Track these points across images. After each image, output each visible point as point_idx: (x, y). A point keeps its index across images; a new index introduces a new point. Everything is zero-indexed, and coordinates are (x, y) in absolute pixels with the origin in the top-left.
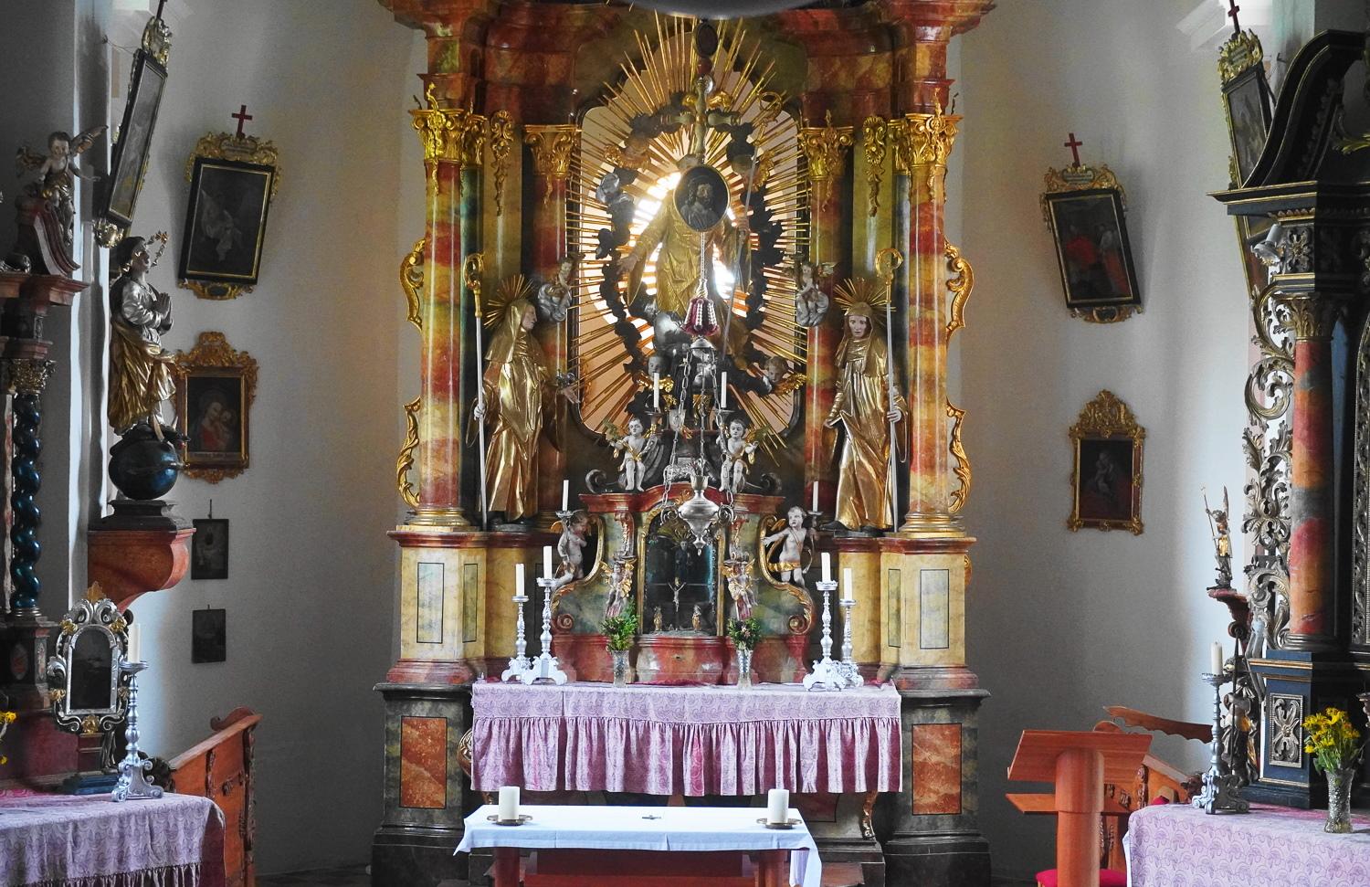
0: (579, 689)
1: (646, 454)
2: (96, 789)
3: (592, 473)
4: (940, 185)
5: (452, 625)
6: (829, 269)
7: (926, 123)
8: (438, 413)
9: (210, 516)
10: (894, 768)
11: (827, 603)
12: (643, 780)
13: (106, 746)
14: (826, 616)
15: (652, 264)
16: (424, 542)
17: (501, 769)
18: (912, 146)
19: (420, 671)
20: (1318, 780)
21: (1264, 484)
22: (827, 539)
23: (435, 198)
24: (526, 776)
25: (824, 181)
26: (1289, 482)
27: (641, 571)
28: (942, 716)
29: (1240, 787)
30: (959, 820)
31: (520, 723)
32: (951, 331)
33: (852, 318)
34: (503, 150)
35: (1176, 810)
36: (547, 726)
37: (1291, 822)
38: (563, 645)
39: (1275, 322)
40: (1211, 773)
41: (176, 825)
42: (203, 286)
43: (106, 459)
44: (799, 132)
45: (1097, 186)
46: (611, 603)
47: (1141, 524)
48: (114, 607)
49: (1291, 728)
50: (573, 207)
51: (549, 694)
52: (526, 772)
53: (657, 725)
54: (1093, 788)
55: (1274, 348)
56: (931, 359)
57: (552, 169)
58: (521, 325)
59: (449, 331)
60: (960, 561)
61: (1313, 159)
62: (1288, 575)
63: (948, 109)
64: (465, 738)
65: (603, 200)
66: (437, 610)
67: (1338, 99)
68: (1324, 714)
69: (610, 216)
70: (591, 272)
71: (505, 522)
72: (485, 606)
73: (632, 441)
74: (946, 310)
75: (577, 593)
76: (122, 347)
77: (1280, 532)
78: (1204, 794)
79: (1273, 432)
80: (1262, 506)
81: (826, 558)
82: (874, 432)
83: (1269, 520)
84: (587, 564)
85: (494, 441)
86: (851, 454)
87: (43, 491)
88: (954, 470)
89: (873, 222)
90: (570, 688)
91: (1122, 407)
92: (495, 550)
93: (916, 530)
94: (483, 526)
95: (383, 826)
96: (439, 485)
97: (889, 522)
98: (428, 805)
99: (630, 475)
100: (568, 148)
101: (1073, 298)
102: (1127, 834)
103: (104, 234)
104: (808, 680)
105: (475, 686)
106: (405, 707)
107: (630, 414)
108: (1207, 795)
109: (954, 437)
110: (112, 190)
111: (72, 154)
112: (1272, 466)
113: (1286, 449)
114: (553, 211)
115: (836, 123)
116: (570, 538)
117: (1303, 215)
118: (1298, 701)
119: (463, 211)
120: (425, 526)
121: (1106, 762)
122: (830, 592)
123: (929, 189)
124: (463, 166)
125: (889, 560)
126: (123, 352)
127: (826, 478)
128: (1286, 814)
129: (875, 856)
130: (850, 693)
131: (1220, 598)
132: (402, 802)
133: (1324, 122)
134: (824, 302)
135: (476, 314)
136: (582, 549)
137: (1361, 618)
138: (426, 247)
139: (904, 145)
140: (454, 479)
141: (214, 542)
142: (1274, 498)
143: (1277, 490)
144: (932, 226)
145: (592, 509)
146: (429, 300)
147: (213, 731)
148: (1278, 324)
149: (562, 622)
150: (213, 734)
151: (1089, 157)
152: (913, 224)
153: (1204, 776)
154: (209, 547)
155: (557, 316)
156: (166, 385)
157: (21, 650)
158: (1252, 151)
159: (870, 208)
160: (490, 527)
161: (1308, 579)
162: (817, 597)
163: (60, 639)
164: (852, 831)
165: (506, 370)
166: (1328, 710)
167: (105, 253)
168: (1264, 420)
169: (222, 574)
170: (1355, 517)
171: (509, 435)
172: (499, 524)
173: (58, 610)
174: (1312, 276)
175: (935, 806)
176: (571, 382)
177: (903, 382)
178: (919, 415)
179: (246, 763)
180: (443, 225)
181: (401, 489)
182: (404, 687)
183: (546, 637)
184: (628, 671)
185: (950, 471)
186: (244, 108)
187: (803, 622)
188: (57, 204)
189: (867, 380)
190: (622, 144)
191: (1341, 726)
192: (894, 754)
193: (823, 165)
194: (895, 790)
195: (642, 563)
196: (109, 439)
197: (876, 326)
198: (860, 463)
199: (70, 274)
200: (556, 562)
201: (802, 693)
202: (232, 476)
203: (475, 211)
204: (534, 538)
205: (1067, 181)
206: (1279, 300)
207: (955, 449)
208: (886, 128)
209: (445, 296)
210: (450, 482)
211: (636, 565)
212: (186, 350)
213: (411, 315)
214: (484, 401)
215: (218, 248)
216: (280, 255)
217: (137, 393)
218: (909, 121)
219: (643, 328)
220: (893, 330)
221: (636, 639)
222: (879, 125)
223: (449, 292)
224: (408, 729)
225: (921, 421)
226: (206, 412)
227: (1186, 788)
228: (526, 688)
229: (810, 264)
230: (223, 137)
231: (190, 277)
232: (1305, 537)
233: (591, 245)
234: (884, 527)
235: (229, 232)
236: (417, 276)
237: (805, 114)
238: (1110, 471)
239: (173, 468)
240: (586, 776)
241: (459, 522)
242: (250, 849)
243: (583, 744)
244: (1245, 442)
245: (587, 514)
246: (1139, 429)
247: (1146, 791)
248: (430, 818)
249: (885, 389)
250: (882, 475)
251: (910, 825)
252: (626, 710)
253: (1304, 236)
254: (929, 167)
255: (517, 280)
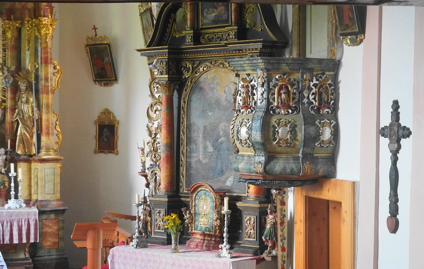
4: (51, 41)
6: (13, 68)
7: (46, 21)
10: (35, 234)
11: (13, 180)
14: (12, 184)
18: (41, 28)
20: (169, 236)
21: (153, 142)
22: (12, 158)
25: (11, 39)
26: (160, 141)
28: (52, 216)
29: (145, 239)
30: (58, 250)
32: (55, 89)
33: (21, 85)
35: (125, 247)
37: (161, 250)
39: (156, 90)
40: (136, 235)
44: (2, 22)
45: (103, 42)
47: (118, 152)
49: (161, 219)
54: (99, 240)
55: (156, 98)
56: (48, 99)
60: (58, 165)
61: (167, 39)
62: (160, 171)
63: (53, 16)
67: (175, 20)
68: (171, 215)
74: (54, 81)
77: (158, 157)
78: (134, 242)
79: (156, 125)
80: (152, 149)
81: (12, 165)
82: (29, 123)
83: (155, 153)
86: (21, 130)
88: (56, 135)
89: (28, 53)
91: (112, 114)
93: (43, 155)
97: (34, 153)
101: (95, 78)
102: (109, 256)
104: (6, 206)
108: (135, 242)
109: (56, 124)
112: (155, 136)
113: (159, 130)
115: (15, 20)
117: (164, 57)
118: (163, 211)
121: (103, 232)
122: (14, 176)
123: (47, 43)
125: (34, 165)
127: (13, 138)
128: (159, 247)
129: (30, 264)
130: (21, 210)
131: (142, 176)
133: (171, 27)
134: (11, 80)
137: (183, 184)
139: (38, 27)
142: (156, 146)
143: (157, 143)
144: (48, 55)
148: (157, 91)
151: (100, 33)
152: (41, 54)
153: (133, 236)
158: (149, 35)
159: (27, 48)
161: (166, 172)
162: (10, 178)
164: (22, 256)
166: (172, 214)
168: (153, 121)
170: (181, 152)
174: (167, 76)
175: (50, 246)
177: (39, 106)
178: (44, 117)
185: (55, 135)
187: (5, 187)
189: (26, 105)
191: (175, 219)
192: (36, 230)
193: (11, 33)
194: (36, 242)
197: (29, 88)
198: (24, 133)
201: (4, 211)
205: (93, 41)
206: (157, 83)
207: (57, 128)
208: (32, 22)
218: (40, 20)
220: (35, 89)
222: (30, 21)
225: (45, 119)
227: (130, 239)
229: (6, 67)
232: (165, 158)
234: (32, 154)
237: (5, 16)
238: (108, 135)
244: (147, 128)
246: (117, 121)
247: (118, 239)
249: (33, 108)
250: (32, 137)
251: (41, 253)
253: (164, 63)
254: (47, 35)
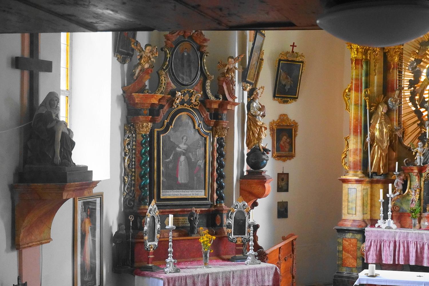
0: (400, 231)
1: (424, 154)
2: (241, 260)
3: (406, 160)
5: (359, 208)
8: (355, 140)
9: (283, 172)
12: (422, 261)
13: (245, 247)
15: (427, 90)
16: (350, 181)
17: (375, 256)
19: (348, 223)
23: (354, 71)
24: (383, 259)
27: (422, 192)
31: (381, 241)
34: (377, 55)
36: (390, 242)
38: (396, 216)
41: (264, 273)
42: (281, 100)
43: (246, 157)
46: (412, 203)
48: (246, 204)
50: (400, 72)
51: (390, 232)
52: (383, 257)
53: (427, 243)
57: (393, 60)
58: (382, 111)
59: (358, 114)
64: (362, 246)
65: (411, 70)
66: (354, 203)
69: (413, 75)
70: (407, 93)
71: (377, 175)
72: (370, 203)
73: (419, 149)
75: (401, 199)
76: (250, 122)
84: (404, 190)
85: (373, 149)
87: (225, 168)
90: (398, 230)
92: (373, 184)
94: (369, 176)
95: (337, 273)
96: (355, 164)
98: (351, 266)
99: (418, 160)
100: (399, 53)
103: (245, 87)
105: (366, 229)
106: (344, 235)
107: (419, 140)
110: (247, 73)
111: (235, 63)
114: (394, 74)
116: (398, 181)
119: (364, 74)
120: (350, 176)
124: (363, 60)
126: (251, 124)
132: (343, 265)
135: (367, 108)
136: (403, 185)
138: (351, 86)
140: (360, 161)
141: (284, 180)
145: (406, 171)
146: (352, 103)
147: (283, 240)
149: (396, 208)
150: (282, 242)
154: (283, 182)
155: (394, 108)
156: (264, 134)
157: (219, 217)
160: (372, 177)
163: (230, 213)
165: (377, 126)
167: (246, 93)
169: (287, 190)
171: (378, 148)
172: (375, 176)
173: (230, 204)
176: (399, 130)
179: (293, 251)
180: (357, 79)
181: (343, 164)
182: (343, 228)
183: (390, 213)
184: (418, 225)
186: (294, 43)
188: (230, 79)
190: (417, 51)
195: (423, 190)
196: (246, 151)
199: (234, 100)
200: (393, 189)
202: (290, 159)
203: (367, 74)
204: (387, 180)
209: (357, 102)
210: (359, 162)
211: (420, 190)
212: (276, 120)
213: (347, 108)
214: (370, 136)
215: (286, 88)
216: (305, 89)
217: (255, 136)
219: (424, 112)
221: (421, 215)
223: (358, 101)
224: (345, 242)
226: (282, 139)
228: (383, 230)
230: (288, 53)
231: (277, 97)
233: (406, 85)
235: (289, 82)
236: (348, 96)
239: (266, 160)
240: (403, 259)
241: (361, 175)
242: (294, 278)
243: (402, 249)
245: (404, 173)
248: (352, 271)
252: (416, 238)
255: (381, 97)
